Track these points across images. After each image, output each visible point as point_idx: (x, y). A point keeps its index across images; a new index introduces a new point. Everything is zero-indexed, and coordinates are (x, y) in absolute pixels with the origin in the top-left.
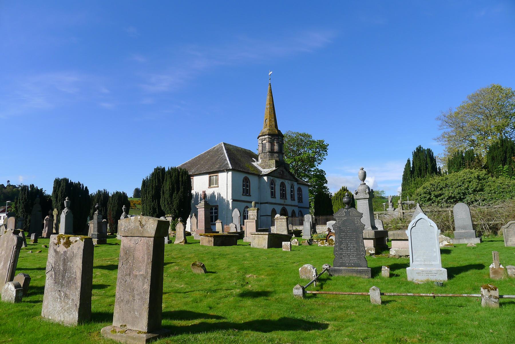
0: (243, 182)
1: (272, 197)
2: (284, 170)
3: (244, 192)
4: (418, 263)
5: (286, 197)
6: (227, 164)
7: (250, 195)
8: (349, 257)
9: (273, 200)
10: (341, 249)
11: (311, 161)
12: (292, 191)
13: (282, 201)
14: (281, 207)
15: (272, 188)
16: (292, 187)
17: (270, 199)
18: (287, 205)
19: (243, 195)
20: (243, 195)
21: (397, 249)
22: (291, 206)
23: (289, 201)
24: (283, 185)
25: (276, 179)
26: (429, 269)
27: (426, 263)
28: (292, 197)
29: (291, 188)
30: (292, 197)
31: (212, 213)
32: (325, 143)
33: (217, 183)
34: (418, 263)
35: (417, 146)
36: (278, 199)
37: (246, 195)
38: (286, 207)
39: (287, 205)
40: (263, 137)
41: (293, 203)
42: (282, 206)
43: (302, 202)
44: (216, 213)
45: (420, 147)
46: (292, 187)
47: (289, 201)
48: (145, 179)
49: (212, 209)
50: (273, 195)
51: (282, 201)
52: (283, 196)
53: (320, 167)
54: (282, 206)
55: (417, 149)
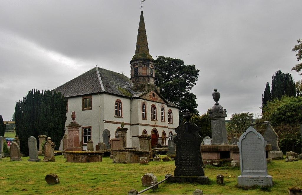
0: (116, 104)
1: (143, 119)
2: (155, 93)
3: (116, 114)
4: (247, 171)
5: (156, 119)
6: (100, 87)
7: (122, 117)
8: (188, 167)
9: (144, 122)
10: (182, 160)
11: (183, 86)
12: (162, 113)
13: (153, 123)
14: (152, 128)
15: (143, 110)
16: (163, 109)
17: (141, 121)
18: (157, 126)
19: (115, 117)
20: (115, 117)
21: (237, 161)
22: (146, 125)
23: (159, 122)
24: (153, 107)
25: (147, 101)
26: (257, 176)
27: (254, 171)
28: (163, 119)
29: (162, 110)
30: (162, 119)
31: (85, 134)
32: (196, 69)
33: (90, 106)
34: (247, 171)
35: (277, 71)
36: (149, 121)
37: (118, 117)
38: (156, 128)
39: (157, 126)
40: (135, 62)
41: (163, 124)
42: (153, 127)
43: (172, 124)
44: (89, 134)
45: (280, 72)
46: (163, 109)
47: (159, 122)
48: (18, 101)
49: (85, 130)
50: (144, 116)
51: (153, 123)
52: (154, 117)
53: (191, 92)
54: (153, 127)
55: (277, 74)
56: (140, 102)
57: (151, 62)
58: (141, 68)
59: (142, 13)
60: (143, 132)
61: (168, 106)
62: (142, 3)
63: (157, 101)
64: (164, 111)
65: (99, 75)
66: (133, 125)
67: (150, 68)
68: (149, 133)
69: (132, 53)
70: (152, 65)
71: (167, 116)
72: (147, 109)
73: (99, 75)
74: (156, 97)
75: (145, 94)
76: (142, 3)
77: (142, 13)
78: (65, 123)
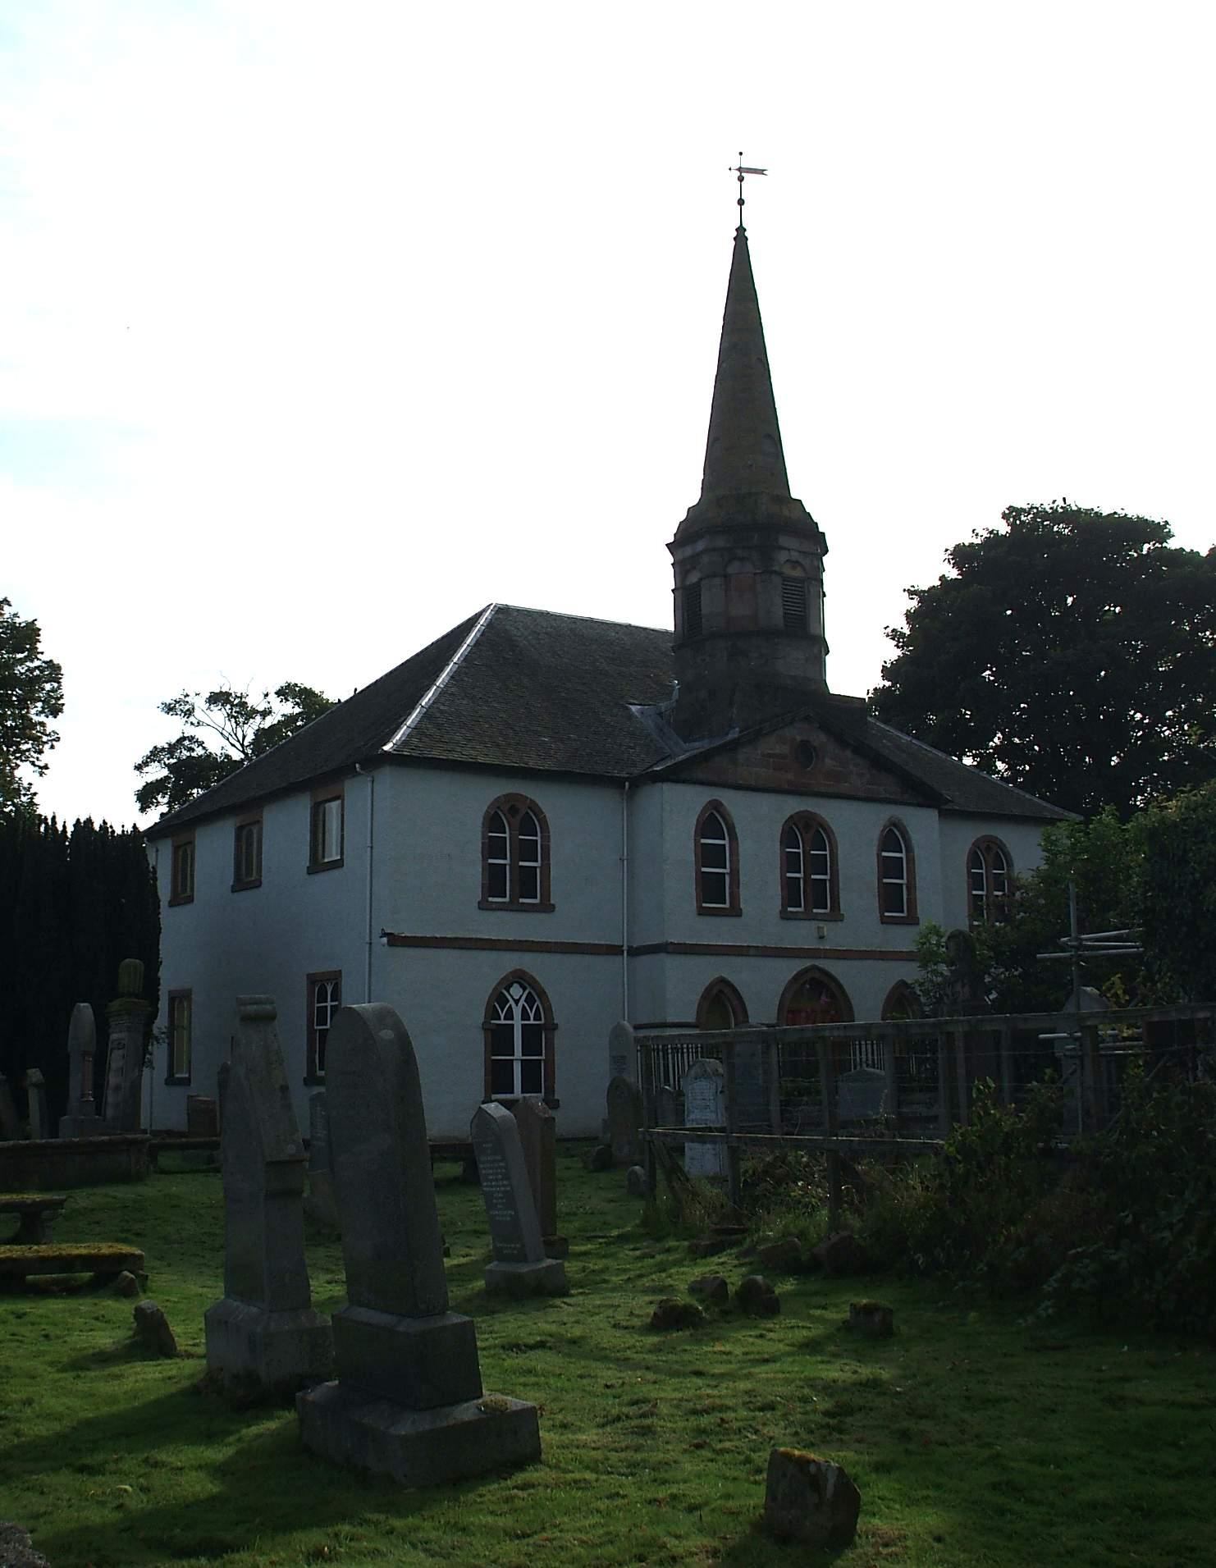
2: (819, 739)
13: (801, 934)
37: (513, 907)
38: (834, 967)
56: (676, 810)
57: (784, 541)
58: (718, 581)
59: (741, 230)
60: (704, 997)
61: (949, 813)
62: (741, 179)
63: (844, 787)
64: (909, 850)
65: (47, 1196)
66: (635, 952)
67: (777, 580)
68: (762, 1009)
69: (681, 486)
70: (795, 555)
71: (775, 890)
72: (746, 846)
73: (47, 1196)
74: (828, 761)
75: (732, 747)
76: (741, 179)
77: (741, 230)
78: (213, 1498)
